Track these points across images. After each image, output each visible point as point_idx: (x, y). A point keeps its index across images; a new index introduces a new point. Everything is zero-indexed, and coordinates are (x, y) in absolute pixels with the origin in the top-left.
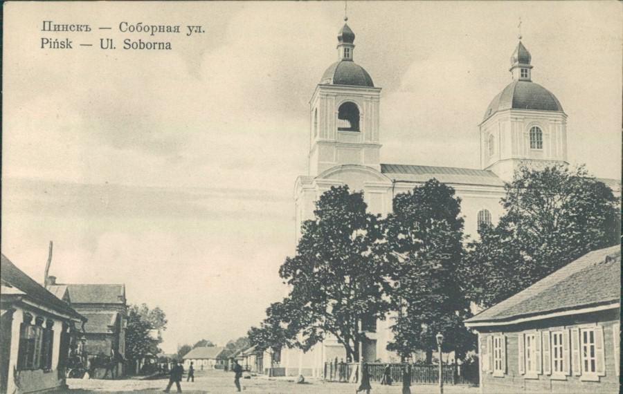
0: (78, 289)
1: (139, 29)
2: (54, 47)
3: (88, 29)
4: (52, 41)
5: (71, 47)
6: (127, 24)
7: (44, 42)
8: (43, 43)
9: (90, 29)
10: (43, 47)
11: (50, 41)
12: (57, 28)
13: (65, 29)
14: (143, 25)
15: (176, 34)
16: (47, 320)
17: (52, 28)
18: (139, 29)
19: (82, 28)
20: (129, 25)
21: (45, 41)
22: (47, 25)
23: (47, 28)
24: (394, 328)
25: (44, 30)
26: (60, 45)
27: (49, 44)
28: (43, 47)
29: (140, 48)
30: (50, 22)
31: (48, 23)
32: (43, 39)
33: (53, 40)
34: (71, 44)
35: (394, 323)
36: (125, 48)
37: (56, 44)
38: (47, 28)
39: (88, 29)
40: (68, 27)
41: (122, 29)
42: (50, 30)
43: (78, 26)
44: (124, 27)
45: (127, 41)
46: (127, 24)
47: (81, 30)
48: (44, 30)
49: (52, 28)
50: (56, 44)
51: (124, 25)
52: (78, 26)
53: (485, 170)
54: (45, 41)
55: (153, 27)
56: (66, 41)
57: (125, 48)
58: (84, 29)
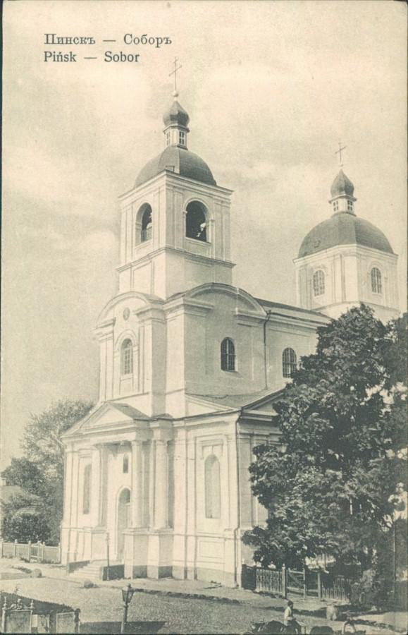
1: (144, 41)
3: (92, 41)
5: (75, 61)
6: (131, 35)
8: (46, 57)
9: (171, 42)
10: (46, 60)
11: (53, 54)
12: (61, 41)
14: (148, 38)
17: (56, 41)
18: (144, 41)
21: (48, 55)
22: (50, 37)
23: (50, 41)
25: (47, 43)
26: (64, 58)
27: (52, 57)
28: (46, 60)
29: (121, 60)
30: (53, 35)
32: (46, 52)
33: (57, 54)
34: (75, 58)
36: (106, 60)
37: (60, 57)
38: (50, 41)
39: (92, 41)
40: (72, 40)
42: (53, 43)
43: (82, 38)
44: (128, 38)
45: (108, 54)
46: (131, 35)
47: (85, 43)
48: (47, 43)
49: (56, 41)
50: (60, 57)
51: (128, 37)
52: (82, 38)
54: (48, 55)
55: (158, 39)
56: (69, 54)
57: (106, 60)
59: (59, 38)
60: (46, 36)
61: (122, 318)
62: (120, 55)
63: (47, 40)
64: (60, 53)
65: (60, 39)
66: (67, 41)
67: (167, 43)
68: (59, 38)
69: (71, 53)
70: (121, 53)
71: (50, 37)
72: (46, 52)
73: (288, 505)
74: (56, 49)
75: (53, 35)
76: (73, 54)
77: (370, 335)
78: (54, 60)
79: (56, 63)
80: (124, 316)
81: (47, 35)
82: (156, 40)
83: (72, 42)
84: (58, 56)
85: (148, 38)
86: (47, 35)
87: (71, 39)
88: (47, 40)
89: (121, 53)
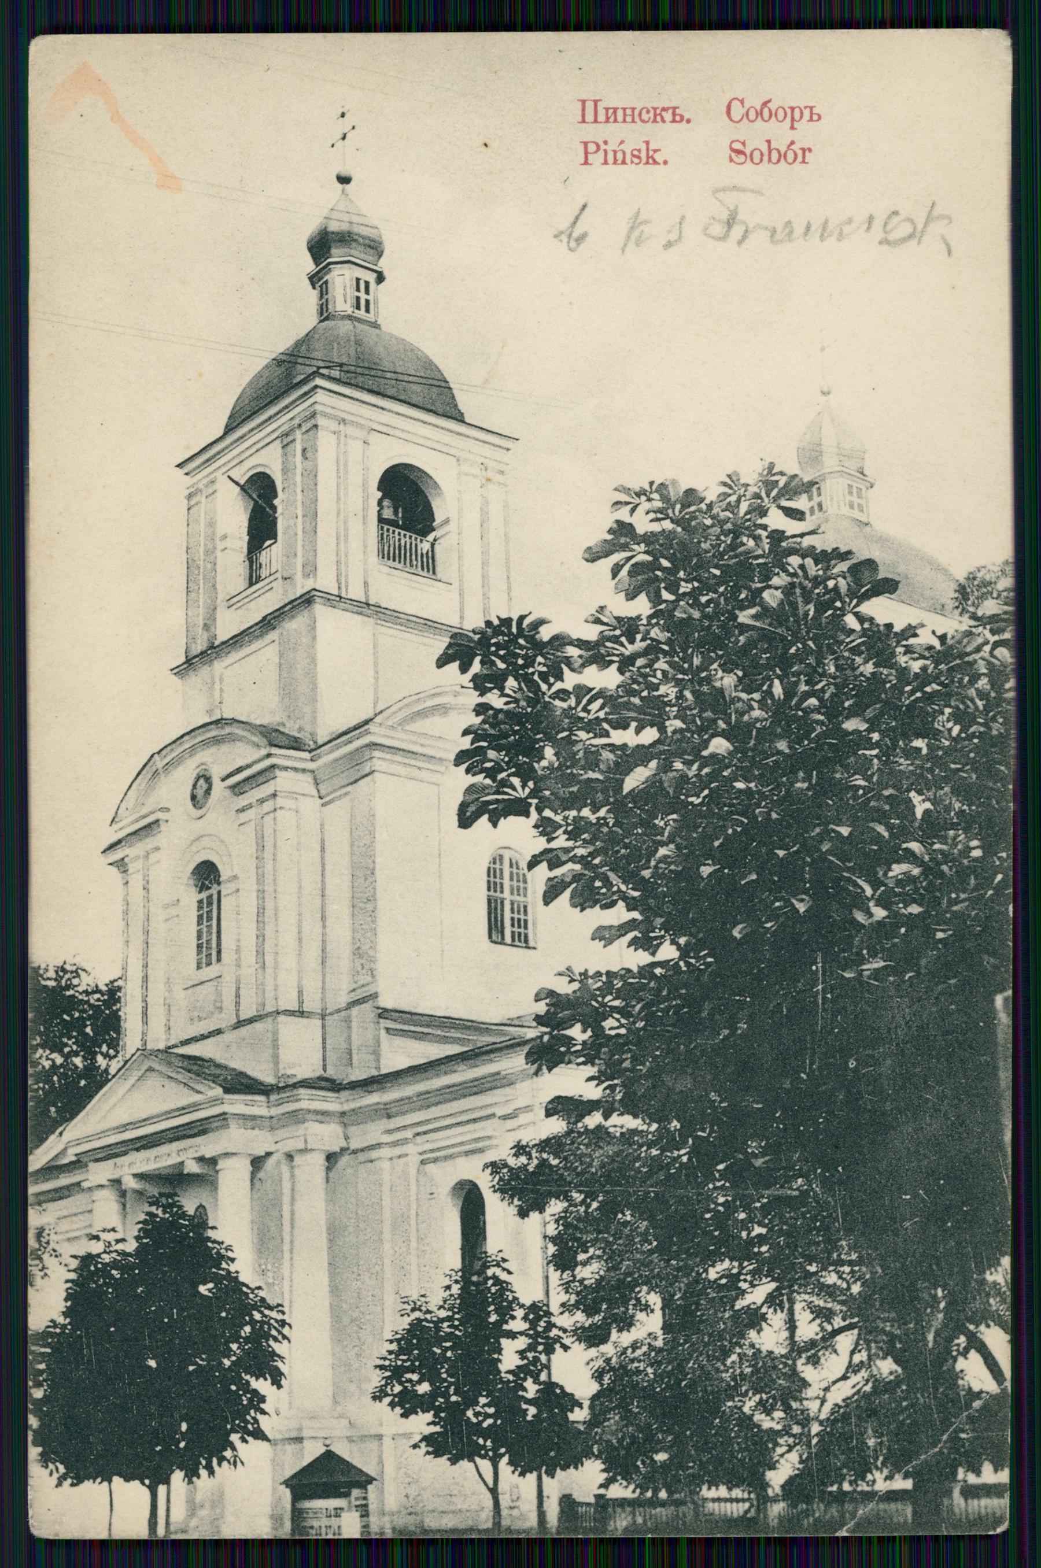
0: (256, 1228)
1: (790, 156)
2: (615, 162)
4: (609, 148)
6: (742, 102)
7: (738, 152)
8: (586, 153)
9: (820, 118)
10: (586, 162)
11: (603, 147)
13: (629, 119)
15: (584, 97)
16: (833, 824)
17: (601, 117)
19: (664, 114)
20: (747, 105)
21: (592, 148)
22: (590, 106)
23: (589, 117)
24: (775, 1310)
25: (584, 121)
27: (601, 153)
28: (586, 162)
29: (770, 160)
30: (596, 102)
31: (592, 103)
32: (586, 144)
33: (612, 146)
35: (771, 1310)
38: (589, 117)
40: (636, 112)
41: (733, 113)
42: (596, 121)
43: (655, 109)
44: (737, 111)
46: (742, 102)
47: (663, 121)
48: (584, 121)
49: (601, 117)
51: (736, 104)
53: (167, 1050)
54: (592, 148)
55: (793, 109)
56: (643, 147)
58: (668, 116)
59: (607, 109)
60: (580, 103)
61: (189, 803)
62: (765, 148)
63: (583, 116)
64: (622, 142)
65: (611, 111)
66: (625, 115)
67: (811, 120)
68: (607, 109)
69: (647, 143)
70: (769, 142)
71: (590, 106)
72: (586, 144)
73: (766, 500)
74: (612, 133)
75: (596, 102)
76: (652, 147)
77: (136, 1436)
78: (606, 163)
79: (611, 167)
80: (193, 797)
81: (584, 102)
82: (789, 111)
83: (637, 119)
84: (615, 152)
85: (773, 106)
86: (584, 102)
87: (633, 109)
88: (583, 116)
89: (769, 142)
